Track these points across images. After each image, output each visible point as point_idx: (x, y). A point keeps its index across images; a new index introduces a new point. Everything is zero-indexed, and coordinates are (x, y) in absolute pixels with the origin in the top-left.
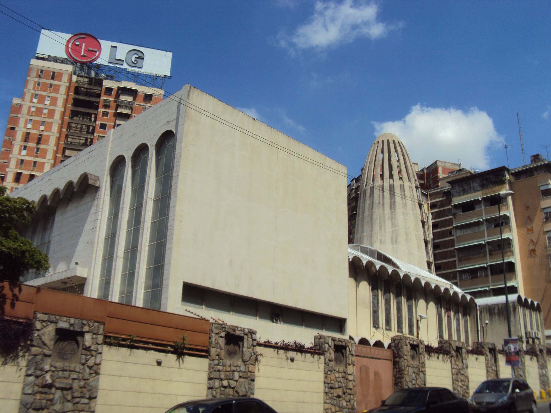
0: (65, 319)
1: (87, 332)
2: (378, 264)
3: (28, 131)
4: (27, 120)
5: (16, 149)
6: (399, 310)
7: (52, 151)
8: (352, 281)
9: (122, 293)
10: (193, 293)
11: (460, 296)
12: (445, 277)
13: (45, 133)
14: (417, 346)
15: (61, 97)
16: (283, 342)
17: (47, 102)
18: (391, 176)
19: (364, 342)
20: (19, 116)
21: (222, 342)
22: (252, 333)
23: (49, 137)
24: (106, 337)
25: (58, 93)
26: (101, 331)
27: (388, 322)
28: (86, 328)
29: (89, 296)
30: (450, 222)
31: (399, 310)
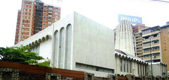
0: (52, 73)
2: (122, 55)
5: (21, 25)
6: (141, 68)
9: (65, 67)
10: (78, 64)
11: (144, 62)
12: (139, 57)
13: (28, 20)
14: (133, 76)
15: (32, 9)
17: (28, 11)
18: (125, 31)
19: (119, 75)
20: (21, 15)
21: (87, 77)
22: (93, 74)
24: (61, 77)
26: (60, 76)
27: (125, 70)
28: (57, 75)
29: (57, 67)
30: (141, 42)
31: (141, 68)
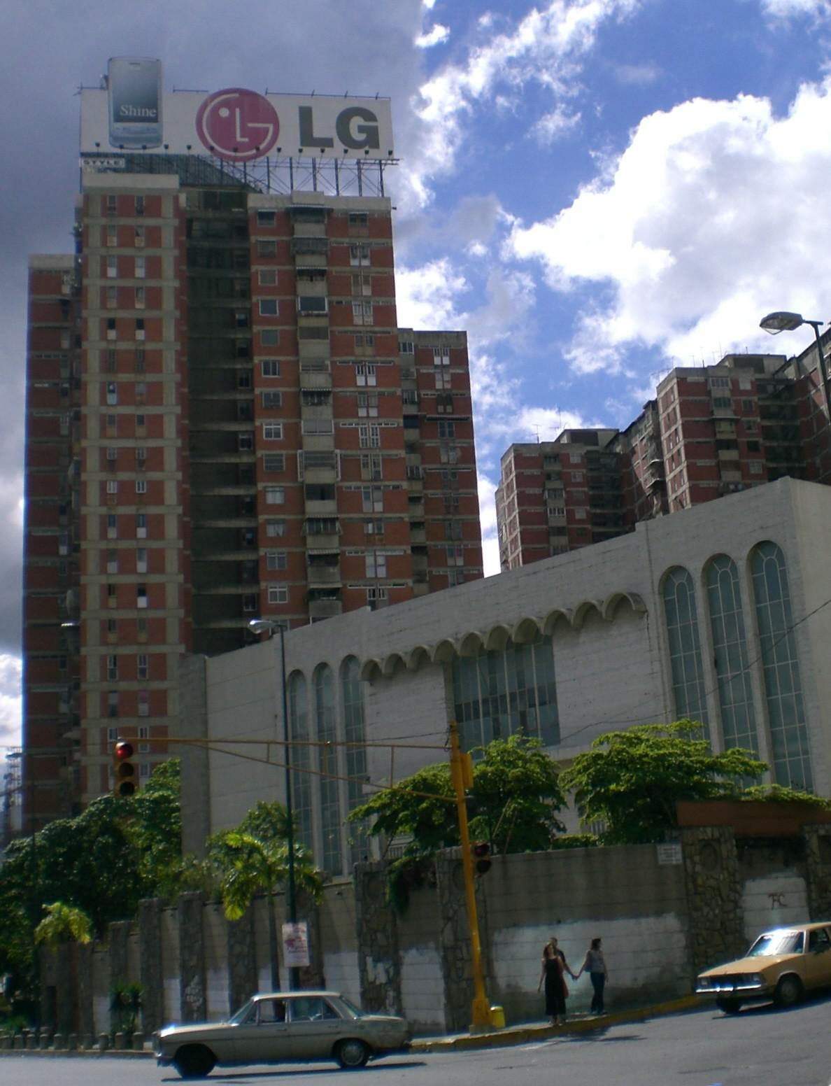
1: (369, 745)
3: (112, 347)
4: (104, 228)
7: (173, 385)
8: (735, 102)
15: (169, 255)
16: (395, 208)
23: (159, 353)
25: (160, 246)
